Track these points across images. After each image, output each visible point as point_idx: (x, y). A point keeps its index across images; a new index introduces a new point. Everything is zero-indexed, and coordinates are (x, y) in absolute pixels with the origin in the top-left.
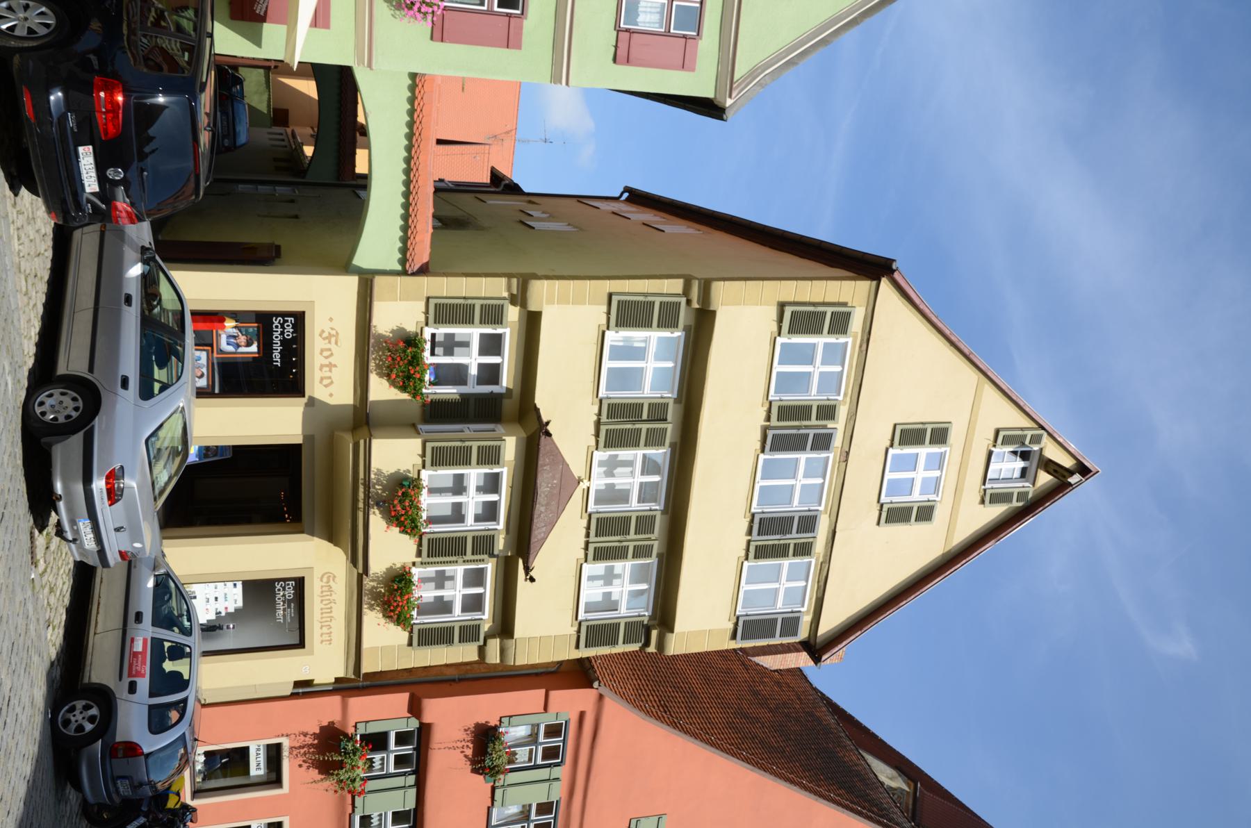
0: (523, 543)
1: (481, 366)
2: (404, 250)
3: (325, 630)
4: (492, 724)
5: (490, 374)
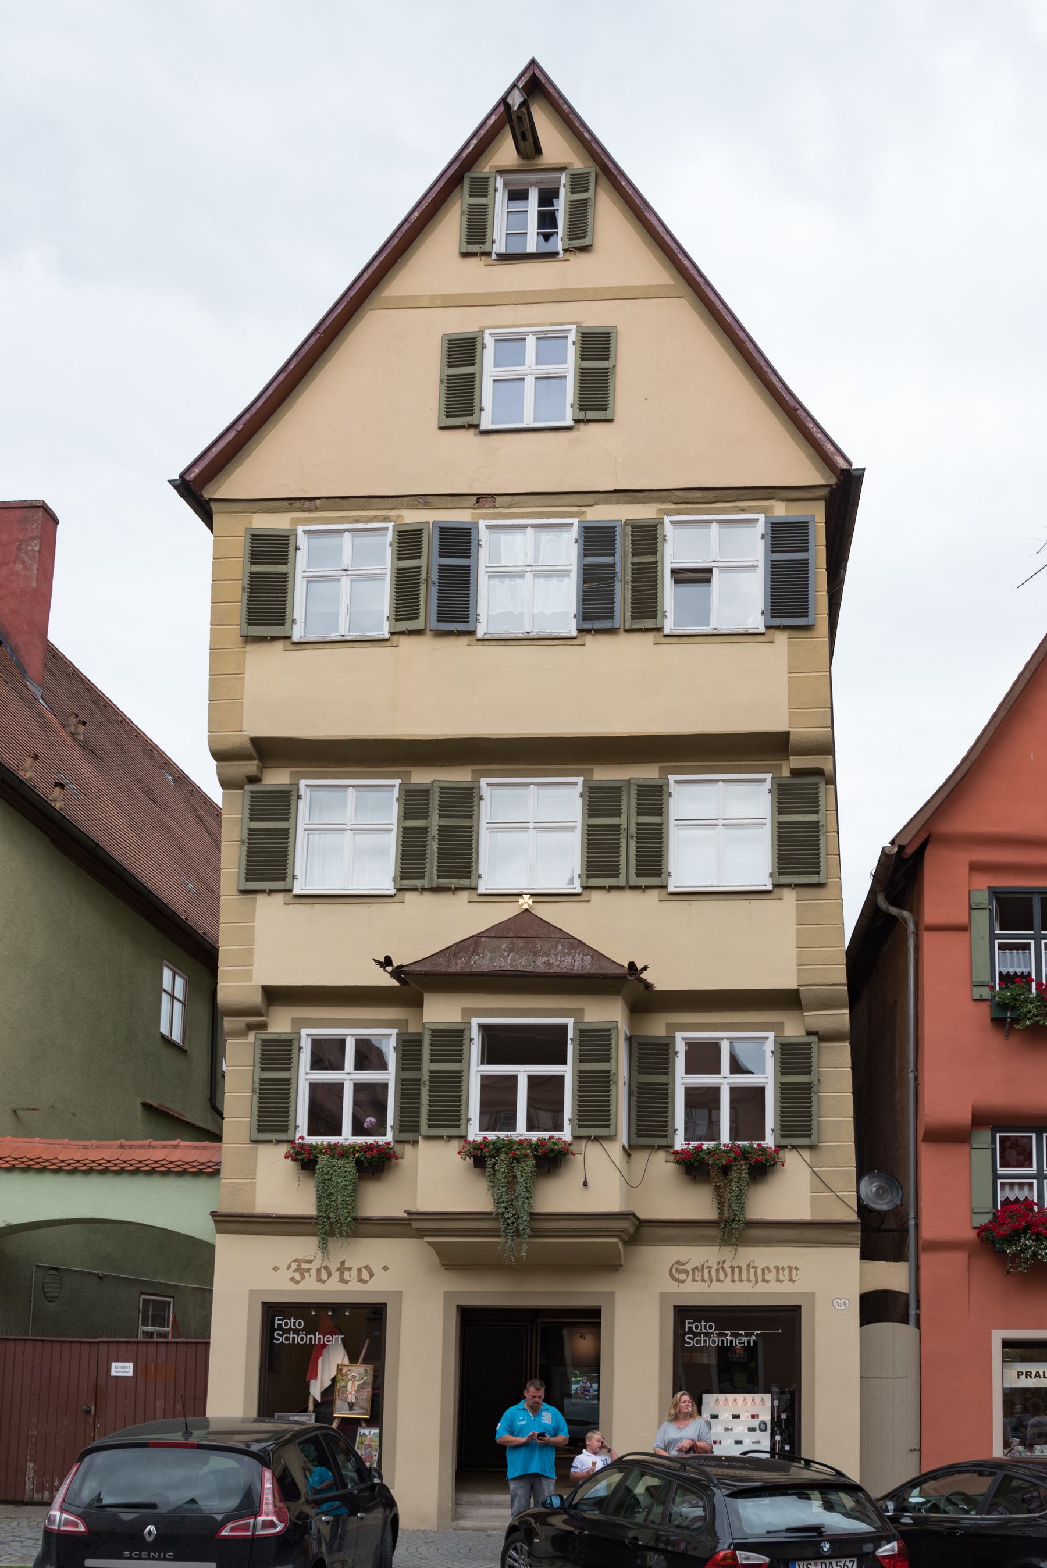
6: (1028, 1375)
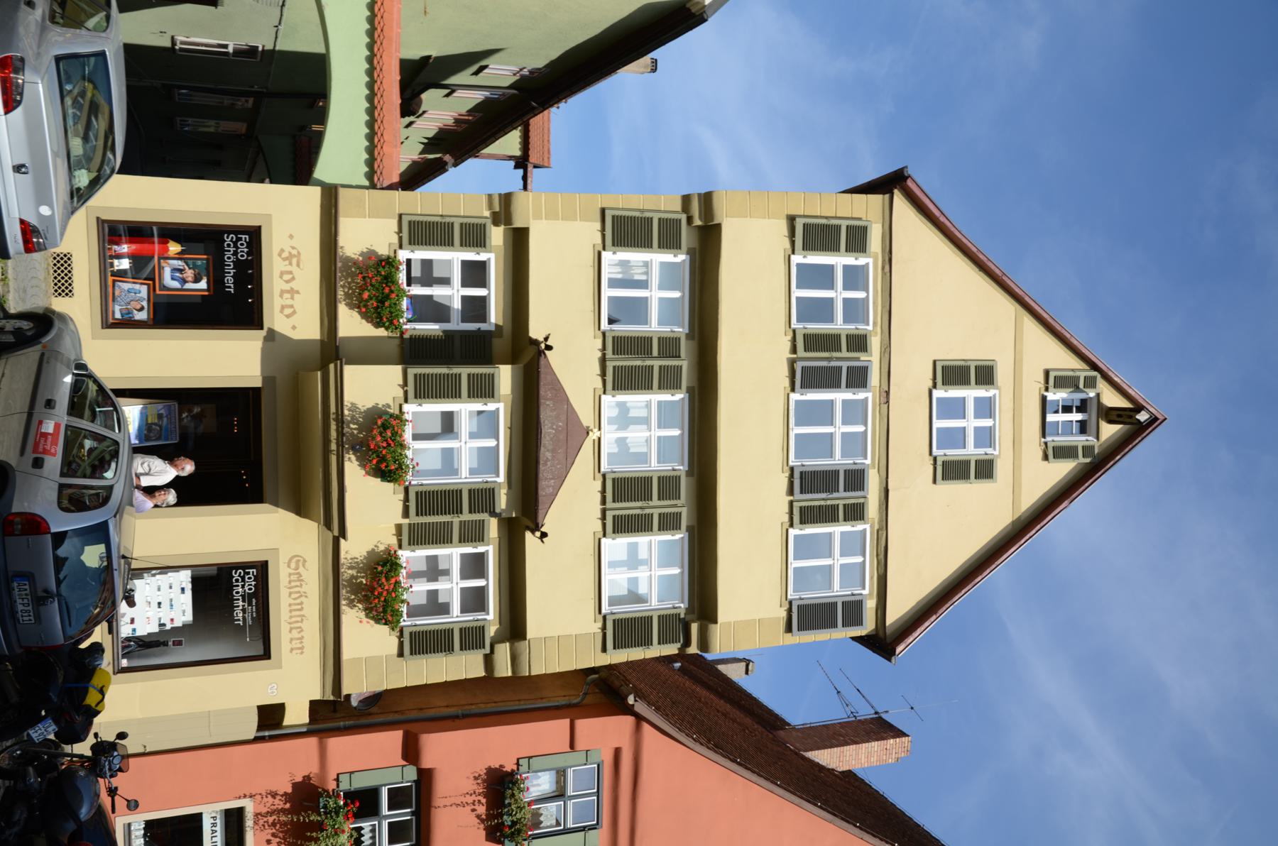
0: (526, 514)
1: (465, 299)
2: (371, 163)
3: (295, 634)
4: (508, 768)
5: (475, 308)
6: (214, 825)
